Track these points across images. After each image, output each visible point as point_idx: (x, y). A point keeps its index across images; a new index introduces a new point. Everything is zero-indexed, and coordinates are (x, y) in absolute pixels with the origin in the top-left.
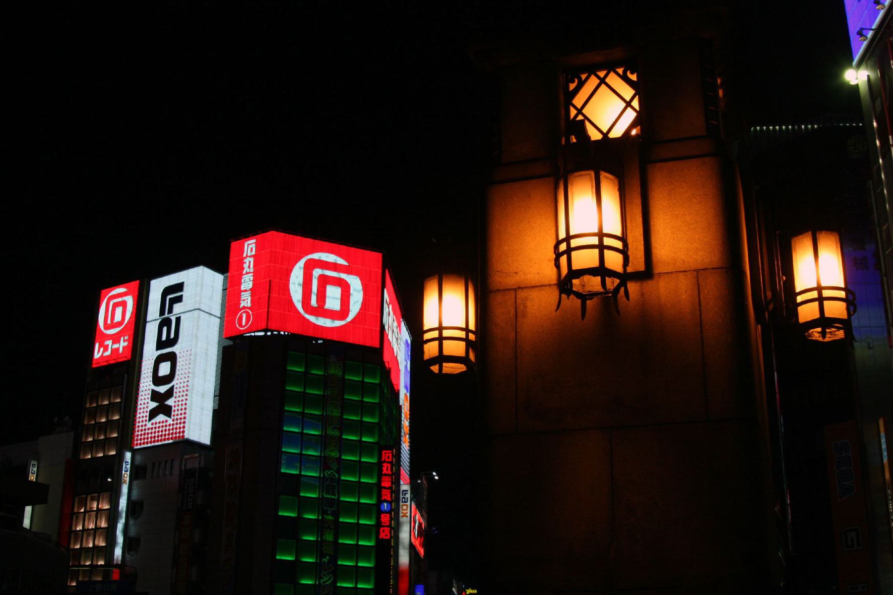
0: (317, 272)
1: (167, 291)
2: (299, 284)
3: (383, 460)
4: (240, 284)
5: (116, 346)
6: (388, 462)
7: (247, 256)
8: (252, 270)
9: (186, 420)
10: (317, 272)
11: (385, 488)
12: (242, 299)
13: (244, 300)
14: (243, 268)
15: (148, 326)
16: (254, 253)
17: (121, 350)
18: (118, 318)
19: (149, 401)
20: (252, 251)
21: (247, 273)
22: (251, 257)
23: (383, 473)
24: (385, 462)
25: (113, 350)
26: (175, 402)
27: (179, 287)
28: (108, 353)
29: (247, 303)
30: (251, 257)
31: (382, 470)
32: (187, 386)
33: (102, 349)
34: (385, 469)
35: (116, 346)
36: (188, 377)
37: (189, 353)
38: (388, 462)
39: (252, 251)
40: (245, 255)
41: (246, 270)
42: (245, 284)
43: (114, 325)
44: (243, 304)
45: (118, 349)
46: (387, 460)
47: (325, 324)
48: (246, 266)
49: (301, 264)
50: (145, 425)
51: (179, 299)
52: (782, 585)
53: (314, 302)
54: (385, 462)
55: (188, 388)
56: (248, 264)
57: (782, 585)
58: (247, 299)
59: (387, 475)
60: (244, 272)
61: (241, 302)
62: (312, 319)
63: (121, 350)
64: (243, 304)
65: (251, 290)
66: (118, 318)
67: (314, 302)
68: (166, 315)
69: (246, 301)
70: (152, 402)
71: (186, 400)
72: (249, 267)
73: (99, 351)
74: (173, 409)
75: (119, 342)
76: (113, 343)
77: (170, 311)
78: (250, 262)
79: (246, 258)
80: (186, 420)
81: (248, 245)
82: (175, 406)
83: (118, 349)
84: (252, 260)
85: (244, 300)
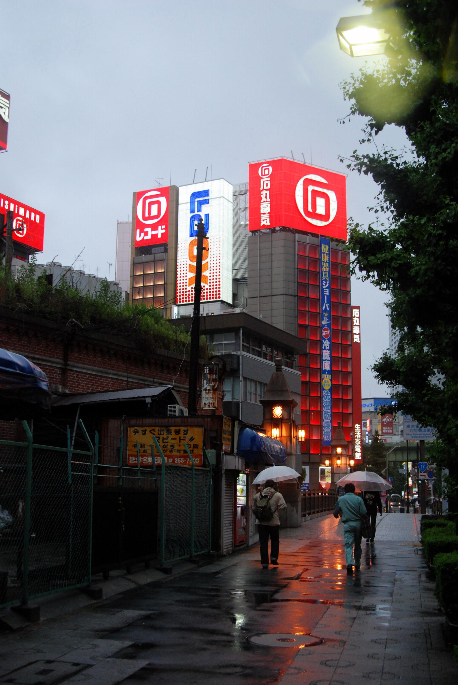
0: (311, 188)
1: (195, 195)
2: (301, 196)
3: (353, 316)
4: (260, 208)
5: (155, 232)
6: (357, 317)
7: (263, 189)
8: (268, 199)
9: (220, 286)
10: (311, 188)
11: (356, 334)
12: (261, 219)
13: (264, 220)
14: (261, 198)
15: (269, 548)
16: (269, 187)
17: (160, 236)
18: (154, 212)
19: (188, 272)
20: (267, 185)
21: (264, 202)
22: (266, 190)
23: (354, 324)
24: (355, 317)
25: (152, 236)
26: (210, 273)
27: (206, 193)
28: (149, 237)
29: (267, 222)
30: (266, 190)
31: (354, 322)
32: (219, 269)
33: (143, 234)
34: (355, 321)
35: (155, 232)
36: (219, 266)
37: (218, 240)
38: (357, 317)
39: (267, 185)
40: (261, 189)
41: (264, 199)
42: (263, 209)
43: (150, 218)
44: (263, 223)
45: (157, 235)
46: (356, 316)
47: (317, 224)
48: (263, 197)
49: (301, 182)
50: (186, 289)
51: (207, 202)
52: (425, 9)
53: (310, 209)
54: (355, 317)
55: (220, 264)
56: (265, 195)
57: (425, 9)
58: (267, 220)
59: (357, 326)
60: (262, 201)
61: (262, 221)
62: (307, 218)
63: (160, 236)
64: (263, 223)
65: (269, 213)
66: (154, 212)
67: (310, 209)
68: (196, 213)
69: (266, 221)
70: (190, 273)
71: (219, 278)
72: (266, 197)
73: (140, 235)
74: (209, 278)
75: (157, 229)
76: (152, 230)
77: (199, 210)
78: (266, 194)
79: (262, 190)
80: (220, 286)
81: (264, 181)
82: (210, 276)
83: (157, 235)
84: (268, 192)
85: (264, 220)
